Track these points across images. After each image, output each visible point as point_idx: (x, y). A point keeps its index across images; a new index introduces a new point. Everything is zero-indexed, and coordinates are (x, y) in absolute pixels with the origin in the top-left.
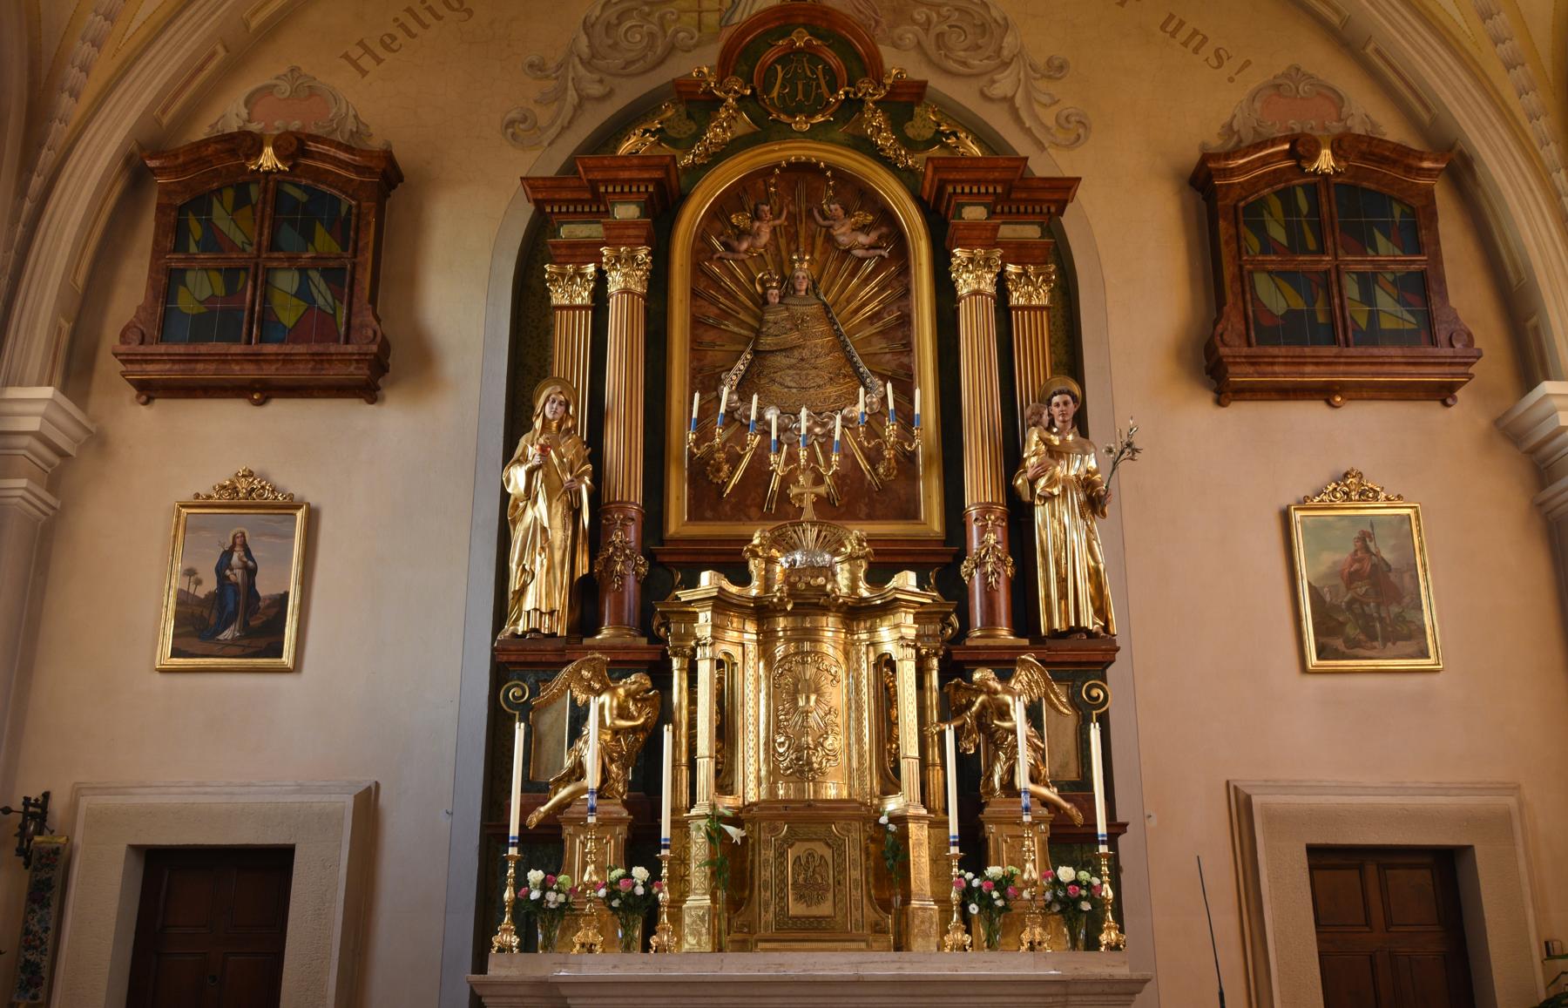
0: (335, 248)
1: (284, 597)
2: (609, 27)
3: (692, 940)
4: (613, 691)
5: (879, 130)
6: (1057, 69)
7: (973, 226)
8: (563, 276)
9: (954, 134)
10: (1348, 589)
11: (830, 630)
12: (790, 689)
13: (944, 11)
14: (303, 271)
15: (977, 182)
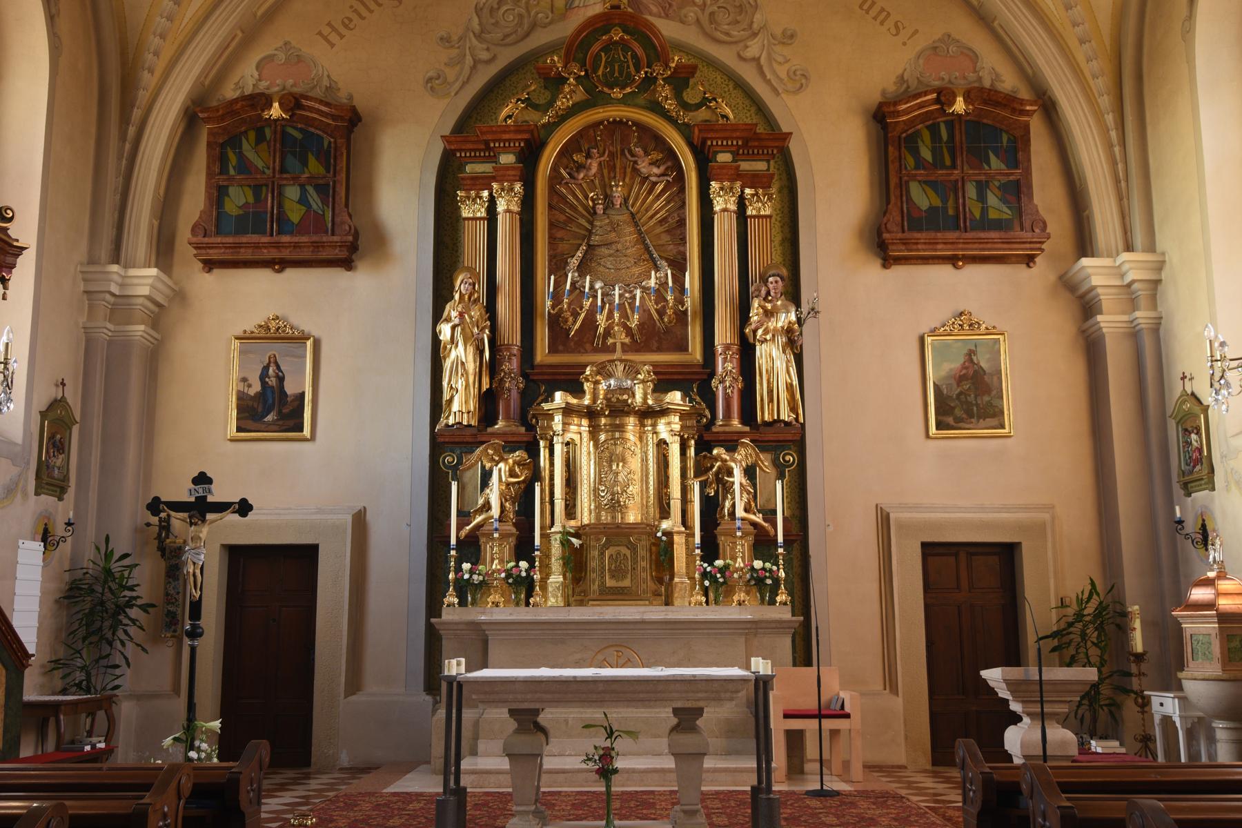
0: (322, 170)
1: (302, 395)
2: (492, 10)
3: (553, 600)
4: (506, 461)
5: (666, 98)
6: (789, 37)
7: (724, 166)
8: (468, 198)
9: (714, 99)
10: (958, 385)
11: (631, 422)
12: (608, 458)
14: (302, 186)
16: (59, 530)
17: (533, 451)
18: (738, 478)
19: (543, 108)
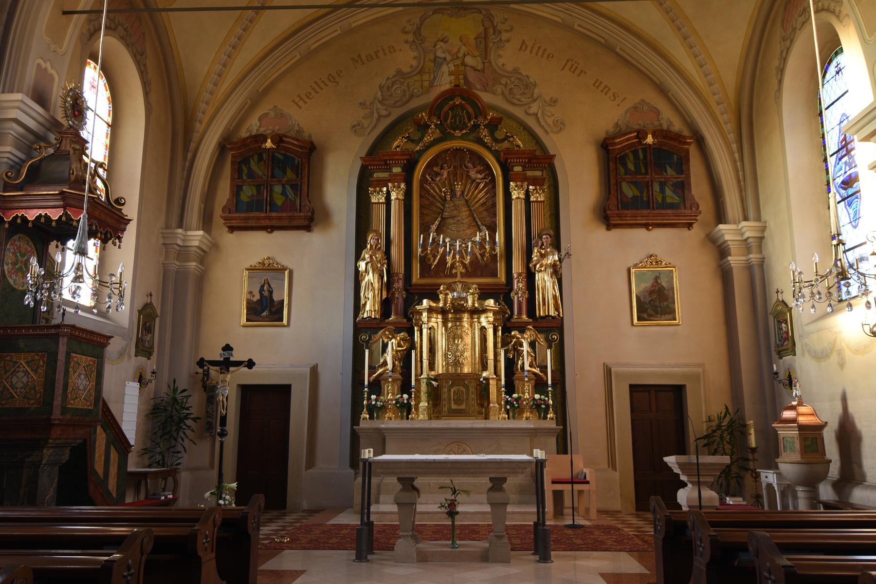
0: (294, 177)
5: (485, 136)
6: (554, 102)
7: (517, 173)
11: (466, 317)
12: (453, 336)
13: (512, 79)
14: (283, 186)
15: (519, 158)
16: (148, 376)
17: (412, 334)
18: (526, 348)
19: (416, 142)
